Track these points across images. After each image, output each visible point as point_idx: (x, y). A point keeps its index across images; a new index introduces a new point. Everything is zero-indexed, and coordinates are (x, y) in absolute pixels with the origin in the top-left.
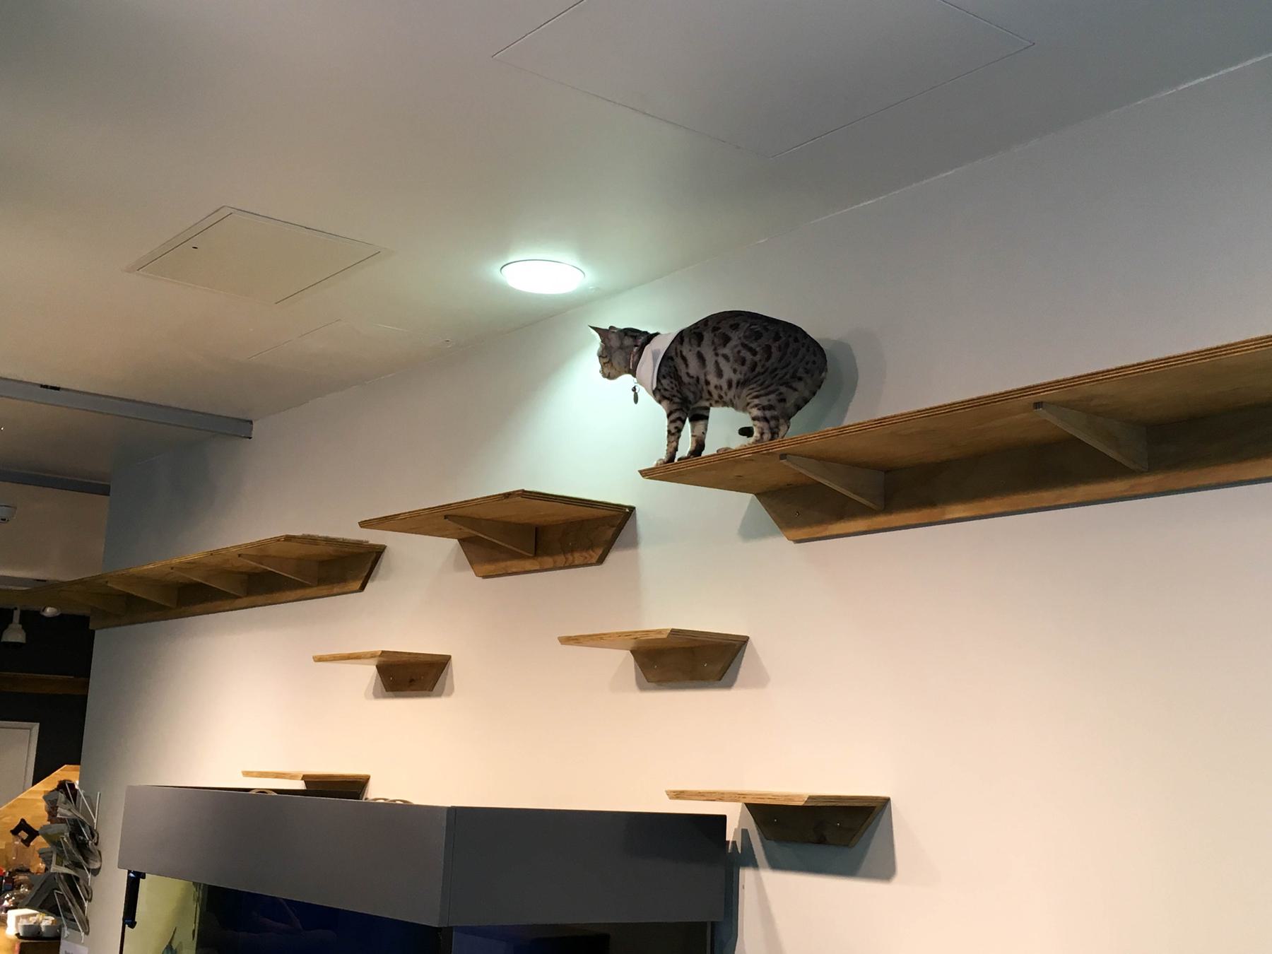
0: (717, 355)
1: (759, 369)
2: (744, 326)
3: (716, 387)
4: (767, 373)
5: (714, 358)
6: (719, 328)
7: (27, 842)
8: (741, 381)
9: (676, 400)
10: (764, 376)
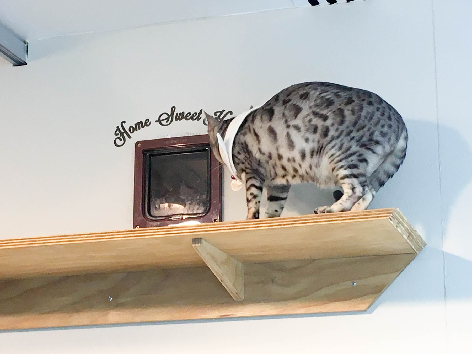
0: (288, 127)
1: (332, 133)
2: (314, 94)
3: (289, 160)
4: (342, 137)
5: (285, 131)
6: (290, 100)
8: (316, 149)
9: (248, 171)
10: (340, 139)
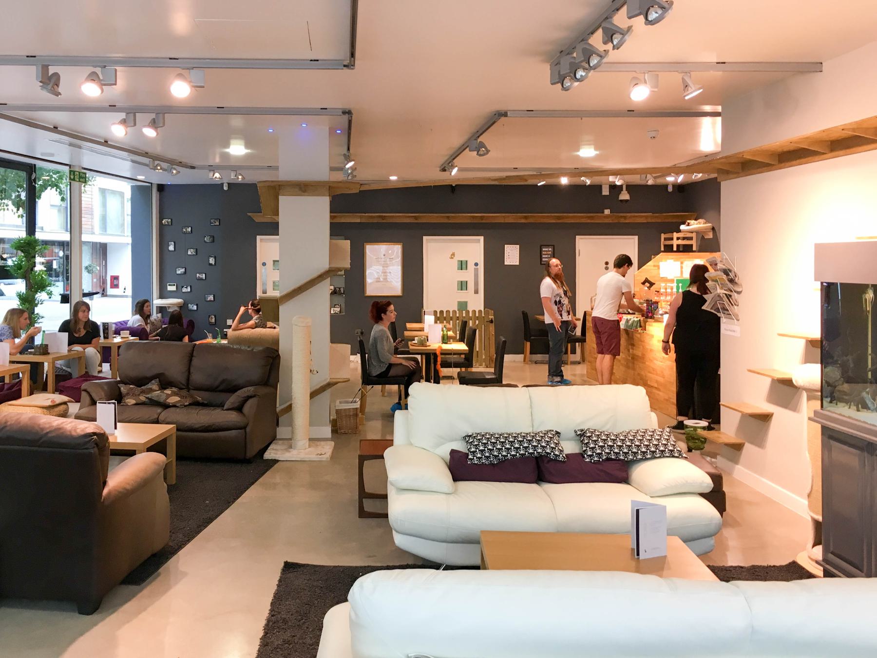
7: (649, 288)
